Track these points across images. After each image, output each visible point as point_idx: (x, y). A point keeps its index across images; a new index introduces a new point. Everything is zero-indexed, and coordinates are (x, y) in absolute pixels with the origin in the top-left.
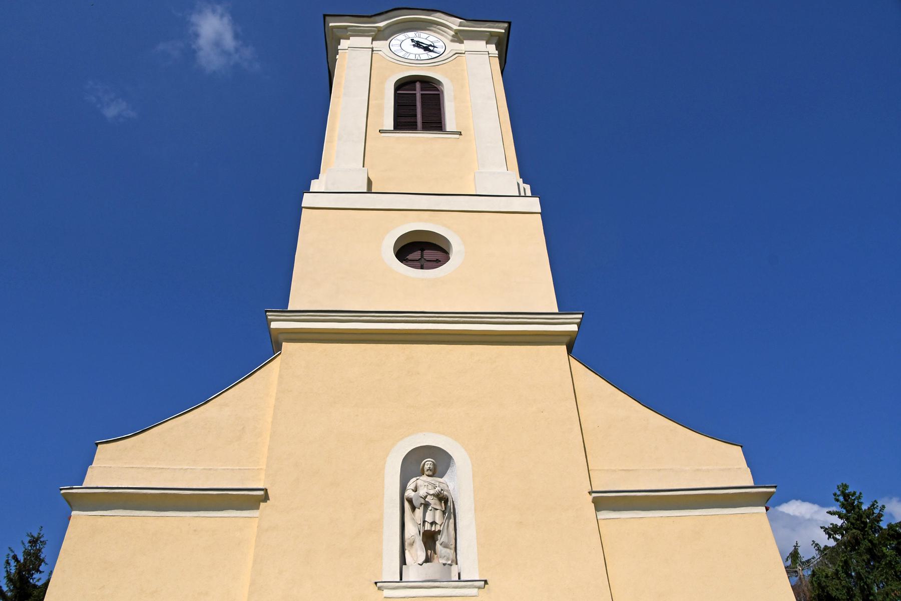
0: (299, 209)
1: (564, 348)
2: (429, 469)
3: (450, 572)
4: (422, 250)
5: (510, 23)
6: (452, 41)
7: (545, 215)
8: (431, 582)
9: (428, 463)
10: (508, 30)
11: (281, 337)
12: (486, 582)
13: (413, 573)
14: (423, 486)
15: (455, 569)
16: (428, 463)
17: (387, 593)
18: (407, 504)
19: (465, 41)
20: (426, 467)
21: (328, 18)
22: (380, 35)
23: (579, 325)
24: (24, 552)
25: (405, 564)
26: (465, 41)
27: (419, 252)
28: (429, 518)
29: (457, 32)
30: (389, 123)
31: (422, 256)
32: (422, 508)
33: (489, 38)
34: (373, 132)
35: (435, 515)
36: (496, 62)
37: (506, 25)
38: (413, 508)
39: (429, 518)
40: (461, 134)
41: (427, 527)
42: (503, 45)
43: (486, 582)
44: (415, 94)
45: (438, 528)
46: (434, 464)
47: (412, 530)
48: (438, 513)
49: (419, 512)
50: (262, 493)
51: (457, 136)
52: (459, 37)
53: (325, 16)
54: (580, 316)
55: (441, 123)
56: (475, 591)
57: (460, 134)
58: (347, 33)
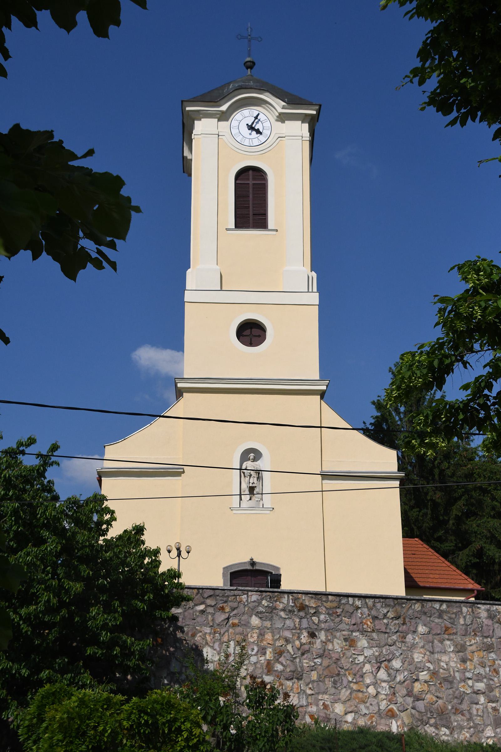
0: (183, 303)
1: (319, 397)
2: (252, 459)
3: (259, 504)
4: (251, 328)
5: (320, 106)
6: (277, 120)
7: (321, 306)
8: (252, 508)
9: (252, 456)
10: (319, 112)
11: (183, 390)
12: (273, 508)
13: (244, 505)
14: (248, 464)
15: (261, 503)
16: (252, 456)
17: (234, 512)
18: (242, 474)
19: (286, 122)
20: (251, 458)
21: (185, 103)
22: (224, 117)
23: (327, 386)
24: (53, 444)
25: (241, 500)
26: (286, 122)
27: (249, 330)
28: (251, 481)
29: (280, 114)
30: (233, 226)
31: (251, 333)
32: (249, 477)
33: (304, 118)
34: (222, 229)
35: (254, 480)
36: (307, 145)
37: (317, 107)
38: (245, 476)
39: (251, 481)
40: (277, 231)
41: (251, 485)
42: (312, 121)
43: (273, 508)
44: (249, 184)
45: (255, 485)
46: (254, 457)
47: (244, 486)
48: (255, 479)
49: (247, 479)
50: (182, 470)
51: (274, 233)
52: (282, 118)
53: (182, 101)
54: (328, 382)
55: (265, 214)
56: (269, 512)
57: (277, 231)
58: (199, 115)
